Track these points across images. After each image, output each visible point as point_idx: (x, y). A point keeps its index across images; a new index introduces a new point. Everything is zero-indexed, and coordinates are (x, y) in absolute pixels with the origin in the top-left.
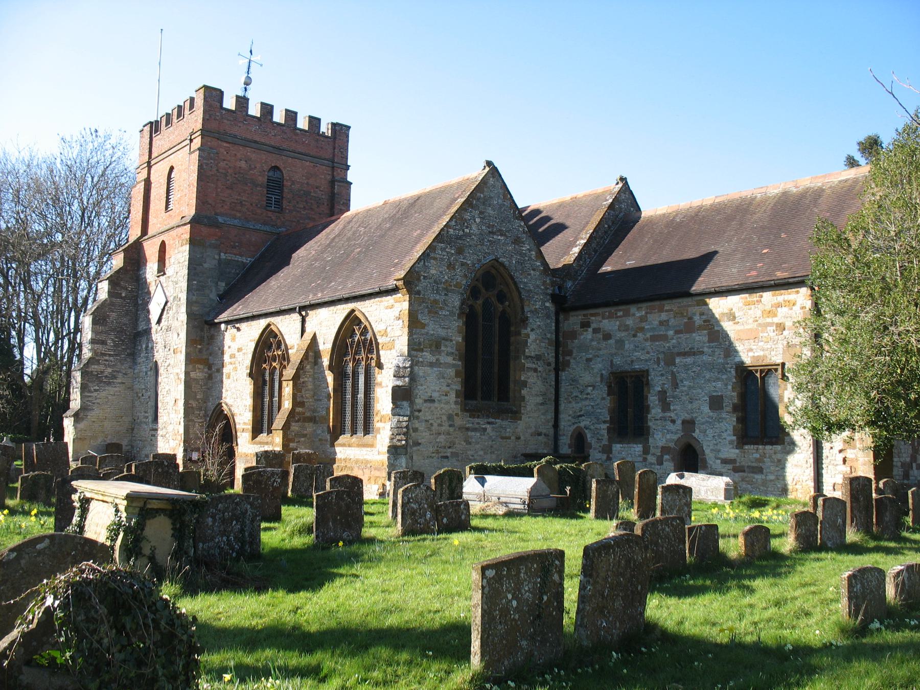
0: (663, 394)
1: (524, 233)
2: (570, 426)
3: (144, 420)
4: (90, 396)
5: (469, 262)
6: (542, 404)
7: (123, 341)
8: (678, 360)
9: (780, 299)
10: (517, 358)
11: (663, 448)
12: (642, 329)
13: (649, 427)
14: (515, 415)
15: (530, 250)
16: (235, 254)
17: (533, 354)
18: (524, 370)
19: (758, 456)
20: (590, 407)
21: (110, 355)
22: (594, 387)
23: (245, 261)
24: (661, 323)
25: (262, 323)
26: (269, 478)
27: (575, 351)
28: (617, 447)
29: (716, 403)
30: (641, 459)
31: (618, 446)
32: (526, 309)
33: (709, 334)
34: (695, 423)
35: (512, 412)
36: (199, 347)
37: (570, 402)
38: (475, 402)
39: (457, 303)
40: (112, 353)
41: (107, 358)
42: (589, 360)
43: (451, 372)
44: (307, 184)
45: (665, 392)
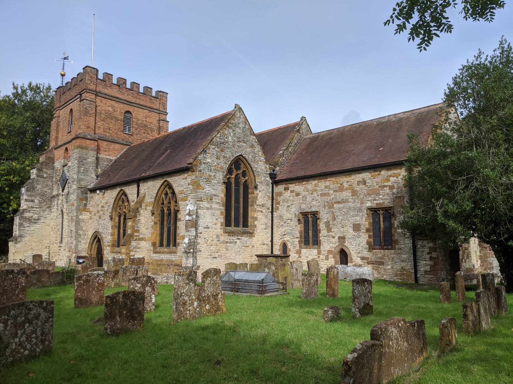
0: (327, 224)
1: (256, 142)
3: (56, 242)
5: (228, 156)
6: (265, 229)
8: (335, 206)
9: (391, 172)
10: (252, 205)
11: (328, 251)
12: (316, 190)
13: (320, 240)
14: (251, 234)
15: (258, 151)
16: (106, 155)
17: (260, 204)
18: (256, 212)
19: (381, 256)
21: (36, 208)
22: (291, 220)
24: (326, 187)
25: (118, 189)
26: (96, 278)
27: (281, 202)
28: (304, 251)
29: (357, 227)
30: (317, 257)
31: (305, 250)
32: (257, 181)
33: (352, 192)
34: (345, 238)
35: (250, 233)
36: (84, 202)
37: (279, 228)
38: (231, 228)
39: (221, 177)
41: (34, 209)
42: (288, 206)
43: (218, 213)
44: (146, 121)
45: (329, 222)
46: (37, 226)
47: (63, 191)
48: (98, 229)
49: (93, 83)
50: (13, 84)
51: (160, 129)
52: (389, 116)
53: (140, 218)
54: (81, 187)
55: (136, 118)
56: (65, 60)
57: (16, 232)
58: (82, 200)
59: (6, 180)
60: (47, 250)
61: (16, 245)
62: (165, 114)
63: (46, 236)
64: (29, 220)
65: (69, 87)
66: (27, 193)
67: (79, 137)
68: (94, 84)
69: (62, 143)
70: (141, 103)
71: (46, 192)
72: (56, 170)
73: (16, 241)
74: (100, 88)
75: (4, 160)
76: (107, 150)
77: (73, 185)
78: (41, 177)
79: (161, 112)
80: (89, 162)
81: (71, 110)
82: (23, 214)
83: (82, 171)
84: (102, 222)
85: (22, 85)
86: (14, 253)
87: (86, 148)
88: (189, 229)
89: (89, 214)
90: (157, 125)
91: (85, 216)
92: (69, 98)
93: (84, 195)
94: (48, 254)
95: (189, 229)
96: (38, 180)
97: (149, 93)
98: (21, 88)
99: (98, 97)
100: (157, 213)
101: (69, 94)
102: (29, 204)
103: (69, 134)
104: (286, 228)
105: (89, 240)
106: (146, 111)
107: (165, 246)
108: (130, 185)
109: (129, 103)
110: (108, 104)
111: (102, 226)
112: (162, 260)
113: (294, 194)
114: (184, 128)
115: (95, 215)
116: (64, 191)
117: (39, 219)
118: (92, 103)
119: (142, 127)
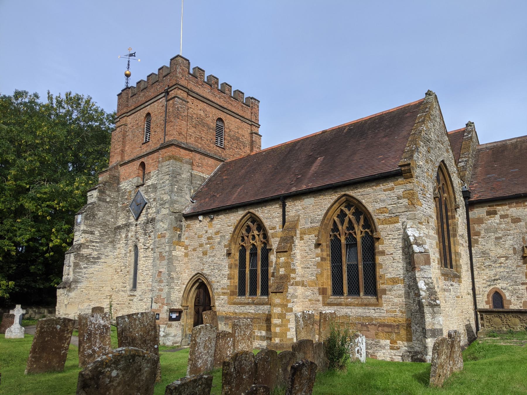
2: (486, 287)
3: (123, 289)
4: (80, 272)
7: (107, 232)
16: (200, 172)
20: (505, 273)
22: (507, 258)
23: (205, 176)
27: (483, 232)
36: (179, 233)
37: (483, 270)
40: (98, 241)
41: (94, 244)
42: (497, 238)
44: (238, 132)
46: (96, 267)
47: (137, 220)
48: (203, 269)
49: (184, 78)
50: (49, 93)
51: (252, 143)
52: (486, 144)
53: (296, 251)
54: (175, 211)
55: (228, 128)
56: (130, 57)
57: (68, 273)
58: (175, 229)
59: (48, 206)
60: (107, 301)
61: (70, 294)
62: (258, 126)
63: (106, 281)
64: (89, 259)
65: (142, 87)
66: (86, 221)
67: (173, 145)
68: (185, 79)
69: (132, 157)
70: (234, 110)
71: (108, 221)
72: (123, 193)
73: (68, 286)
74: (191, 86)
75: (44, 180)
76: (200, 165)
77: (163, 209)
78: (103, 202)
79: (253, 123)
80: (183, 178)
81: (148, 114)
82: (80, 251)
83: (175, 190)
84: (210, 260)
85: (58, 96)
86: (66, 305)
87: (179, 160)
88: (422, 267)
89: (183, 250)
90: (249, 139)
91: (179, 252)
92: (143, 100)
93: (179, 223)
94: (109, 306)
95: (422, 267)
96: (99, 206)
97: (241, 99)
98: (56, 99)
99: (189, 96)
100: (326, 243)
101: (144, 95)
102: (88, 237)
103: (145, 145)
104: (498, 270)
105: (185, 286)
106: (238, 120)
107: (345, 295)
108: (265, 206)
109: (221, 108)
110: (199, 107)
111: (210, 266)
112: (347, 316)
113: (509, 220)
114: (324, 132)
115: (194, 250)
116: (140, 219)
117: (99, 258)
118: (184, 102)
119: (234, 140)
